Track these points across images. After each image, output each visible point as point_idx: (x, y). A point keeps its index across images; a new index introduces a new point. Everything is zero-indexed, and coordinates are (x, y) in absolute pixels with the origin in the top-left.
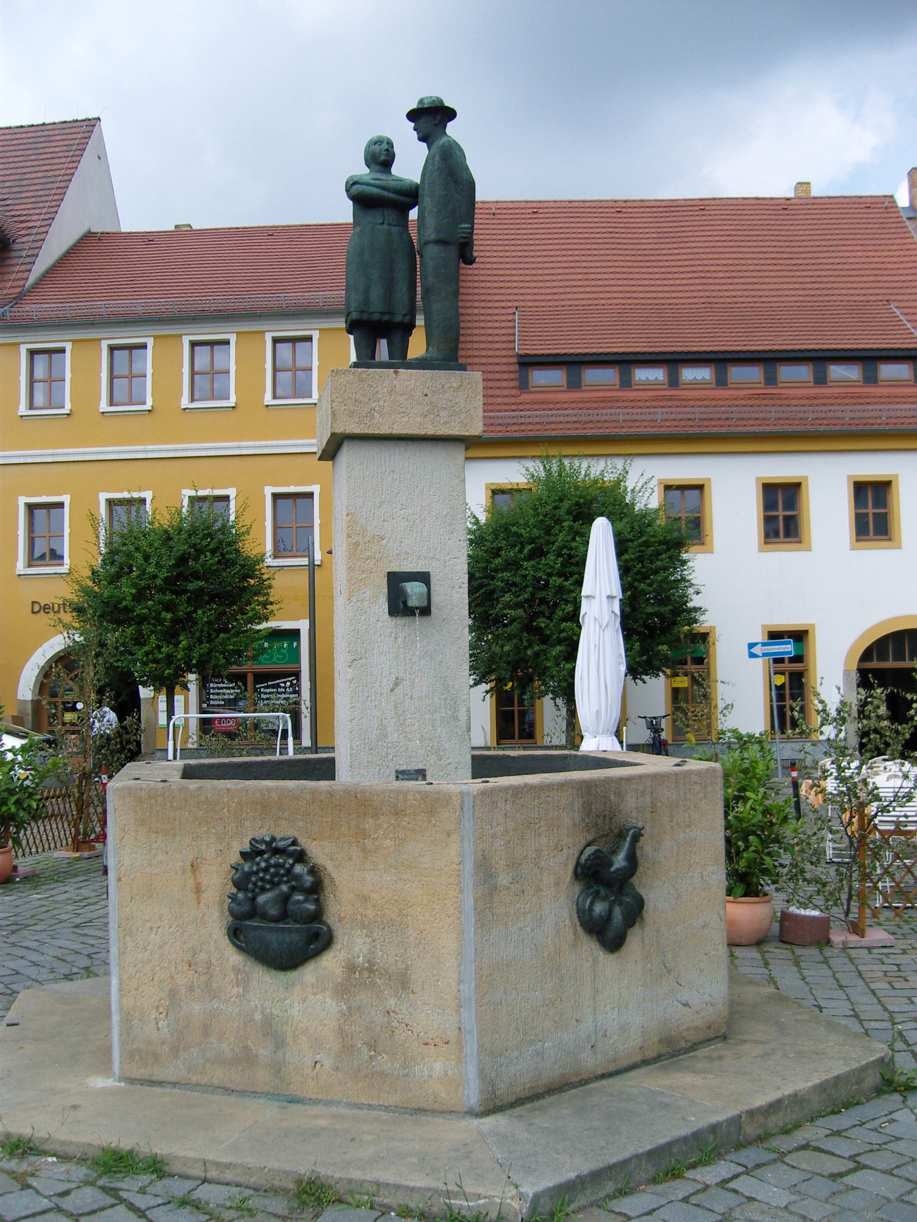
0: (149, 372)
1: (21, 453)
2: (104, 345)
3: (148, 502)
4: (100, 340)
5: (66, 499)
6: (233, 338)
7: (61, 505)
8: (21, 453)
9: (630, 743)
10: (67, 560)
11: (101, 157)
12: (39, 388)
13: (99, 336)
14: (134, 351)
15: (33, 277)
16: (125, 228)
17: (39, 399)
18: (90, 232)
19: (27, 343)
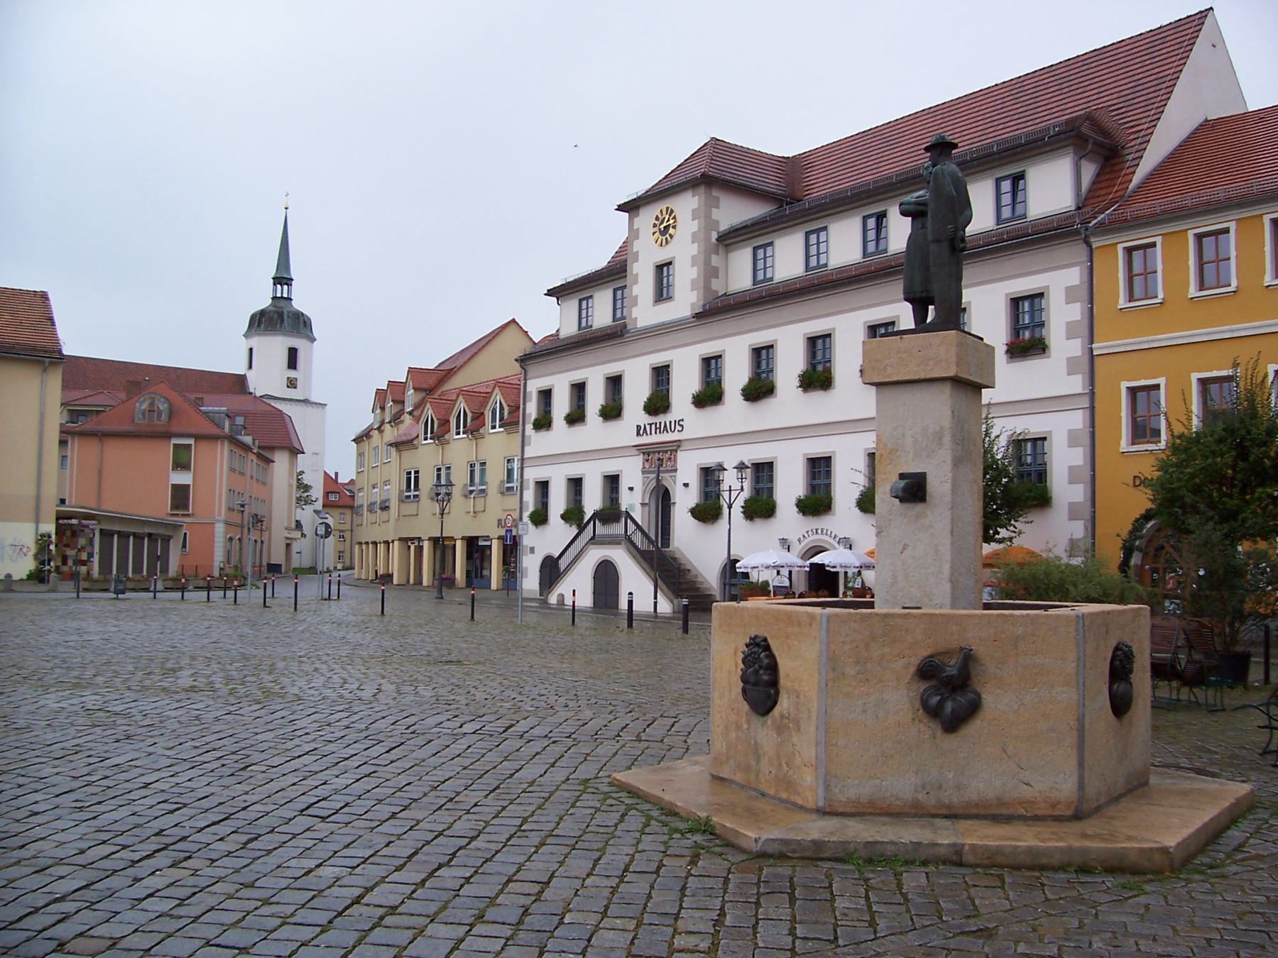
0: (1233, 254)
1: (1146, 339)
2: (1191, 234)
3: (1162, 387)
4: (1186, 230)
5: (1161, 381)
6: (1232, 226)
7: (1157, 387)
8: (1146, 339)
9: (948, 600)
10: (1164, 436)
11: (1218, 44)
12: (1138, 281)
13: (1115, 241)
14: (1220, 237)
15: (1137, 179)
16: (1252, 106)
17: (1138, 291)
18: (1206, 120)
19: (1123, 242)
